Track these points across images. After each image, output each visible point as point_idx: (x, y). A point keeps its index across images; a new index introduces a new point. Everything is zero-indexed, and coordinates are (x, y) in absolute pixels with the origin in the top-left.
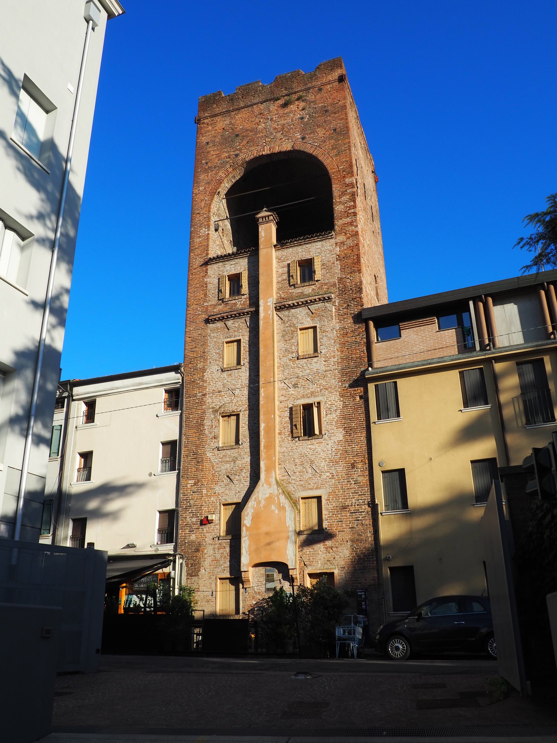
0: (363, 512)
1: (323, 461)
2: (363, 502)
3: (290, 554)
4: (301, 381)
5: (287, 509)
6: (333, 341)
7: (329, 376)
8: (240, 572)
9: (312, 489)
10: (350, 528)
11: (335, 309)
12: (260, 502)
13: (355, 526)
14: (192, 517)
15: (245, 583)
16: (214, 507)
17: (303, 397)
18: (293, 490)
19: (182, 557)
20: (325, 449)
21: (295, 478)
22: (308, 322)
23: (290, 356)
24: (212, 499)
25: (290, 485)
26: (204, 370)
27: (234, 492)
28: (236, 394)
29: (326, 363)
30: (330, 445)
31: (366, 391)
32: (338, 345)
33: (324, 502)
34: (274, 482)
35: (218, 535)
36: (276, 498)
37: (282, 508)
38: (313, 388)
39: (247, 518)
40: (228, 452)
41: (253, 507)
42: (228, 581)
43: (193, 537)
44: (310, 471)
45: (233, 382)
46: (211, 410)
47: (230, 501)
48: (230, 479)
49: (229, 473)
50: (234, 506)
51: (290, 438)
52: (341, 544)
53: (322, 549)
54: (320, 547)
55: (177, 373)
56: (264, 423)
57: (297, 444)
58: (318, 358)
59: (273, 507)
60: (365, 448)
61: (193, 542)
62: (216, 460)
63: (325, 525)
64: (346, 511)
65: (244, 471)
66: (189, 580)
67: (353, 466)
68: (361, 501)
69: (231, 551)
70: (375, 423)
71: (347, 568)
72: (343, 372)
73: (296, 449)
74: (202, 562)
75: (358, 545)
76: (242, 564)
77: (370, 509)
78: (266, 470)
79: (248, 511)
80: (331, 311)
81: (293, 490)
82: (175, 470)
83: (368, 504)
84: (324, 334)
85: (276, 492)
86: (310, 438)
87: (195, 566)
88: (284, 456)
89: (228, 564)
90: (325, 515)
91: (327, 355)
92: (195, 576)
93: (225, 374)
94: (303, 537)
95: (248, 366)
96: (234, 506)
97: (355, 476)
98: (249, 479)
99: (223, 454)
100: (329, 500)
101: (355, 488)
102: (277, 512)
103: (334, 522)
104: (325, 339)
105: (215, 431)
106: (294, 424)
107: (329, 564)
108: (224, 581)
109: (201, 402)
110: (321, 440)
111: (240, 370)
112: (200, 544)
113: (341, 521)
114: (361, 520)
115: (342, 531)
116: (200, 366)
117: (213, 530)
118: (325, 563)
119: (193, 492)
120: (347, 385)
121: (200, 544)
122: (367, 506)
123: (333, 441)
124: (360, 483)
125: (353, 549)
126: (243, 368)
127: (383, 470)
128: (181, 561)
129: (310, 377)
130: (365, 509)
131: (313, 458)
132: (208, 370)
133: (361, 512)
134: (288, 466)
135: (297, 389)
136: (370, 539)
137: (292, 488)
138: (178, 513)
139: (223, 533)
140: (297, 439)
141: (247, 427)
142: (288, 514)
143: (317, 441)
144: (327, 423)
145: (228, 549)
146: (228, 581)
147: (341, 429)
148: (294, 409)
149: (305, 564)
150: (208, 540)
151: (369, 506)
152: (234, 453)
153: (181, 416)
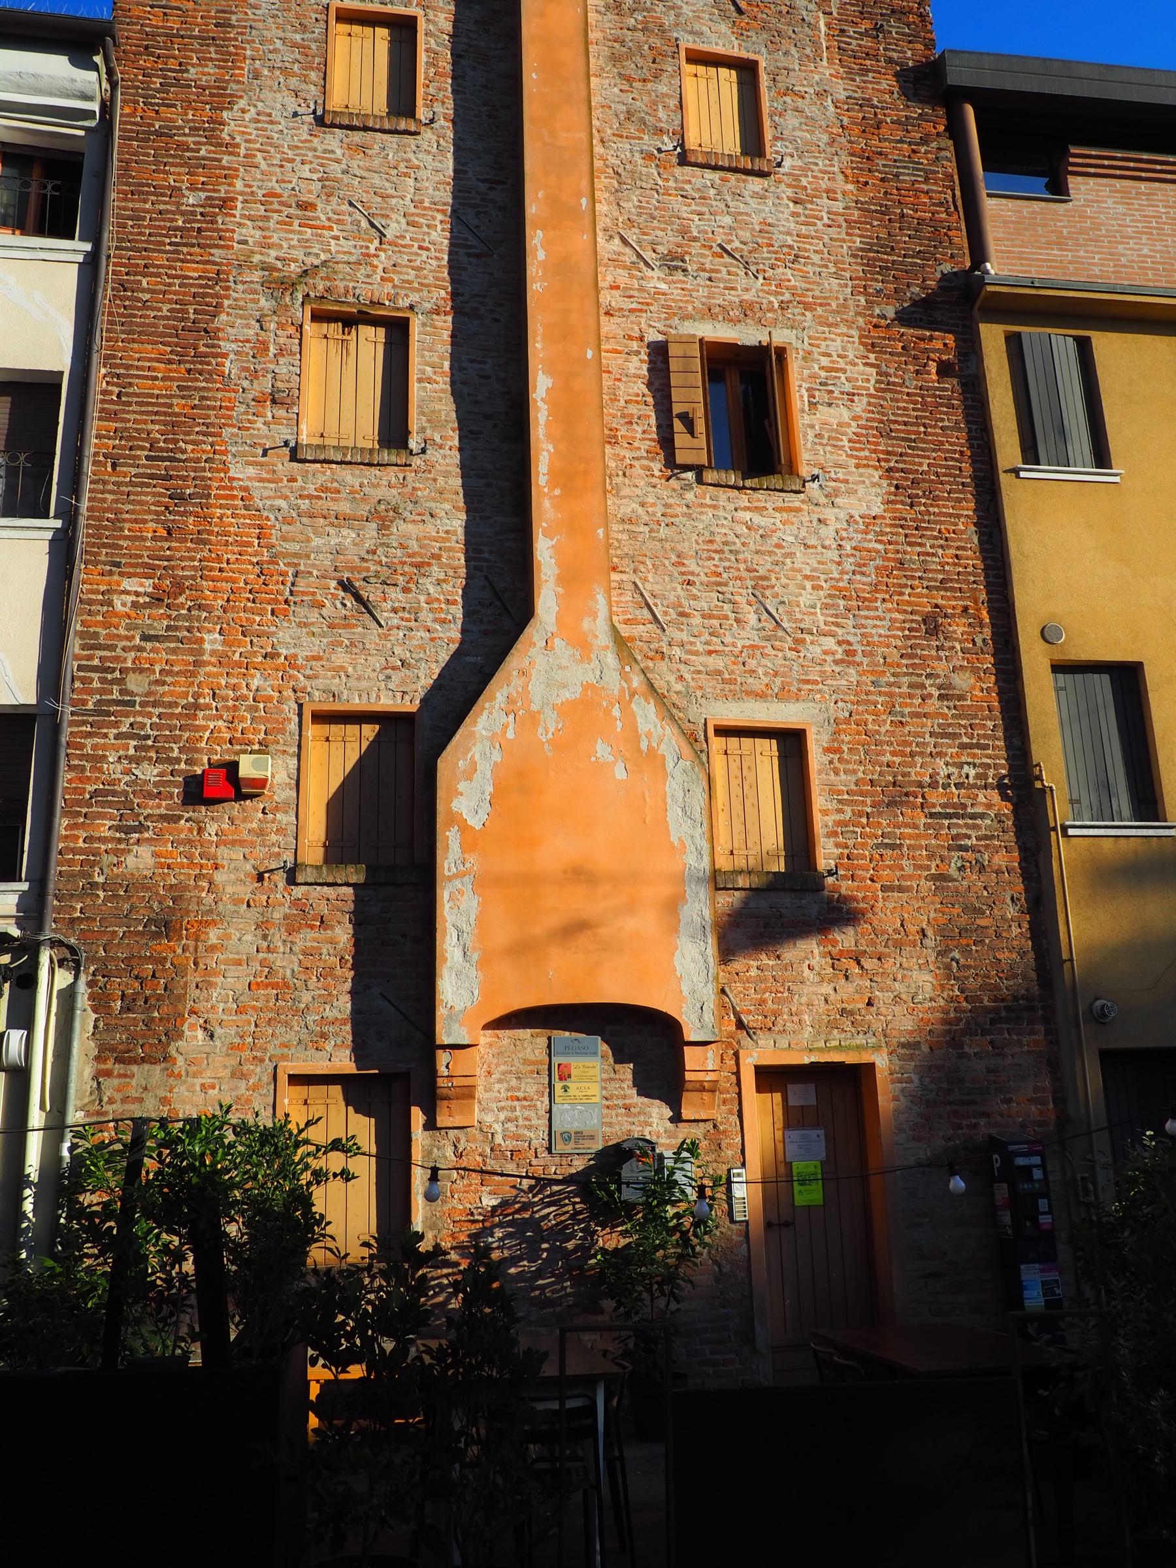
0: (982, 816)
1: (808, 585)
2: (977, 776)
3: (684, 979)
4: (696, 248)
5: (670, 764)
6: (825, 138)
7: (816, 258)
8: (428, 1046)
9: (761, 696)
10: (934, 878)
11: (828, 25)
12: (533, 718)
13: (953, 871)
14: (137, 761)
15: (442, 1107)
16: (262, 720)
17: (709, 313)
18: (678, 687)
19: (71, 959)
20: (812, 541)
21: (684, 636)
22: (721, 35)
23: (649, 142)
24: (256, 683)
25: (663, 666)
26: (220, 98)
27: (377, 662)
28: (390, 234)
29: (799, 209)
30: (832, 529)
31: (970, 349)
32: (845, 158)
33: (816, 758)
34: (603, 638)
35: (289, 857)
36: (616, 712)
37: (647, 760)
38: (749, 289)
39: (469, 782)
40: (349, 476)
41: (498, 740)
42: (336, 1091)
43: (140, 859)
44: (752, 618)
45: (377, 180)
46: (257, 276)
47: (357, 703)
48: (358, 598)
49: (352, 569)
50: (370, 731)
51: (657, 466)
52: (898, 945)
53: (816, 961)
54: (808, 954)
55: (82, 60)
56: (549, 372)
57: (690, 496)
58: (765, 182)
59: (602, 750)
60: (973, 561)
61: (133, 885)
62: (282, 503)
63: (826, 854)
64: (914, 807)
65: (436, 572)
66: (110, 1084)
67: (932, 625)
68: (972, 773)
69: (359, 942)
70: (1016, 471)
71: (925, 1048)
72: (876, 261)
73: (689, 516)
74: (193, 993)
75: (966, 952)
76: (441, 1012)
77: (1006, 809)
78: (561, 580)
79: (476, 751)
80: (814, 27)
81: (678, 687)
82: (42, 512)
83: (1001, 787)
84: (788, 99)
85: (613, 681)
86: (748, 483)
87: (149, 1009)
88: (633, 536)
89: (345, 1004)
90: (825, 813)
91: (804, 182)
92: (153, 1061)
93: (334, 140)
94: (729, 900)
95: (450, 134)
96: (370, 731)
97: (941, 667)
98: (458, 611)
99: (321, 479)
100: (839, 751)
101: (944, 716)
102: (620, 773)
103: (864, 845)
104: (791, 121)
105: (282, 370)
106: (677, 409)
107: (848, 1027)
108: (313, 1089)
109: (204, 229)
110: (794, 500)
111: (410, 139)
112: (177, 893)
113: (892, 847)
114: (973, 849)
115: (901, 889)
116: (200, 73)
117: (261, 833)
118: (832, 1025)
119: (145, 638)
120: (890, 312)
121: (177, 893)
122: (995, 796)
123: (843, 515)
124: (961, 698)
125: (948, 967)
126: (428, 134)
127: (1058, 656)
128: (63, 979)
129: (737, 244)
130: (989, 806)
131: (764, 565)
132: (242, 103)
133: (973, 816)
134: (652, 584)
135: (679, 275)
136: (1015, 931)
137: (672, 679)
138: (56, 729)
139: (313, 848)
140: (690, 476)
141: (443, 383)
142: (673, 786)
143: (778, 499)
144: (817, 436)
145: (343, 934)
146: (336, 1091)
147: (877, 474)
148: (673, 350)
149: (740, 1025)
150: (232, 878)
151: (1004, 797)
152: (382, 484)
153: (90, 270)
